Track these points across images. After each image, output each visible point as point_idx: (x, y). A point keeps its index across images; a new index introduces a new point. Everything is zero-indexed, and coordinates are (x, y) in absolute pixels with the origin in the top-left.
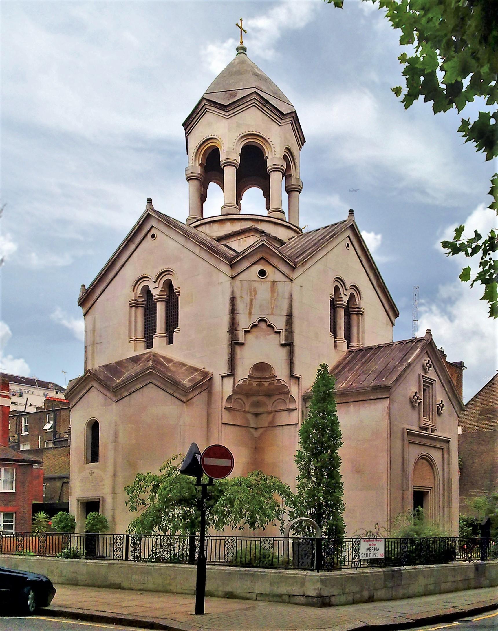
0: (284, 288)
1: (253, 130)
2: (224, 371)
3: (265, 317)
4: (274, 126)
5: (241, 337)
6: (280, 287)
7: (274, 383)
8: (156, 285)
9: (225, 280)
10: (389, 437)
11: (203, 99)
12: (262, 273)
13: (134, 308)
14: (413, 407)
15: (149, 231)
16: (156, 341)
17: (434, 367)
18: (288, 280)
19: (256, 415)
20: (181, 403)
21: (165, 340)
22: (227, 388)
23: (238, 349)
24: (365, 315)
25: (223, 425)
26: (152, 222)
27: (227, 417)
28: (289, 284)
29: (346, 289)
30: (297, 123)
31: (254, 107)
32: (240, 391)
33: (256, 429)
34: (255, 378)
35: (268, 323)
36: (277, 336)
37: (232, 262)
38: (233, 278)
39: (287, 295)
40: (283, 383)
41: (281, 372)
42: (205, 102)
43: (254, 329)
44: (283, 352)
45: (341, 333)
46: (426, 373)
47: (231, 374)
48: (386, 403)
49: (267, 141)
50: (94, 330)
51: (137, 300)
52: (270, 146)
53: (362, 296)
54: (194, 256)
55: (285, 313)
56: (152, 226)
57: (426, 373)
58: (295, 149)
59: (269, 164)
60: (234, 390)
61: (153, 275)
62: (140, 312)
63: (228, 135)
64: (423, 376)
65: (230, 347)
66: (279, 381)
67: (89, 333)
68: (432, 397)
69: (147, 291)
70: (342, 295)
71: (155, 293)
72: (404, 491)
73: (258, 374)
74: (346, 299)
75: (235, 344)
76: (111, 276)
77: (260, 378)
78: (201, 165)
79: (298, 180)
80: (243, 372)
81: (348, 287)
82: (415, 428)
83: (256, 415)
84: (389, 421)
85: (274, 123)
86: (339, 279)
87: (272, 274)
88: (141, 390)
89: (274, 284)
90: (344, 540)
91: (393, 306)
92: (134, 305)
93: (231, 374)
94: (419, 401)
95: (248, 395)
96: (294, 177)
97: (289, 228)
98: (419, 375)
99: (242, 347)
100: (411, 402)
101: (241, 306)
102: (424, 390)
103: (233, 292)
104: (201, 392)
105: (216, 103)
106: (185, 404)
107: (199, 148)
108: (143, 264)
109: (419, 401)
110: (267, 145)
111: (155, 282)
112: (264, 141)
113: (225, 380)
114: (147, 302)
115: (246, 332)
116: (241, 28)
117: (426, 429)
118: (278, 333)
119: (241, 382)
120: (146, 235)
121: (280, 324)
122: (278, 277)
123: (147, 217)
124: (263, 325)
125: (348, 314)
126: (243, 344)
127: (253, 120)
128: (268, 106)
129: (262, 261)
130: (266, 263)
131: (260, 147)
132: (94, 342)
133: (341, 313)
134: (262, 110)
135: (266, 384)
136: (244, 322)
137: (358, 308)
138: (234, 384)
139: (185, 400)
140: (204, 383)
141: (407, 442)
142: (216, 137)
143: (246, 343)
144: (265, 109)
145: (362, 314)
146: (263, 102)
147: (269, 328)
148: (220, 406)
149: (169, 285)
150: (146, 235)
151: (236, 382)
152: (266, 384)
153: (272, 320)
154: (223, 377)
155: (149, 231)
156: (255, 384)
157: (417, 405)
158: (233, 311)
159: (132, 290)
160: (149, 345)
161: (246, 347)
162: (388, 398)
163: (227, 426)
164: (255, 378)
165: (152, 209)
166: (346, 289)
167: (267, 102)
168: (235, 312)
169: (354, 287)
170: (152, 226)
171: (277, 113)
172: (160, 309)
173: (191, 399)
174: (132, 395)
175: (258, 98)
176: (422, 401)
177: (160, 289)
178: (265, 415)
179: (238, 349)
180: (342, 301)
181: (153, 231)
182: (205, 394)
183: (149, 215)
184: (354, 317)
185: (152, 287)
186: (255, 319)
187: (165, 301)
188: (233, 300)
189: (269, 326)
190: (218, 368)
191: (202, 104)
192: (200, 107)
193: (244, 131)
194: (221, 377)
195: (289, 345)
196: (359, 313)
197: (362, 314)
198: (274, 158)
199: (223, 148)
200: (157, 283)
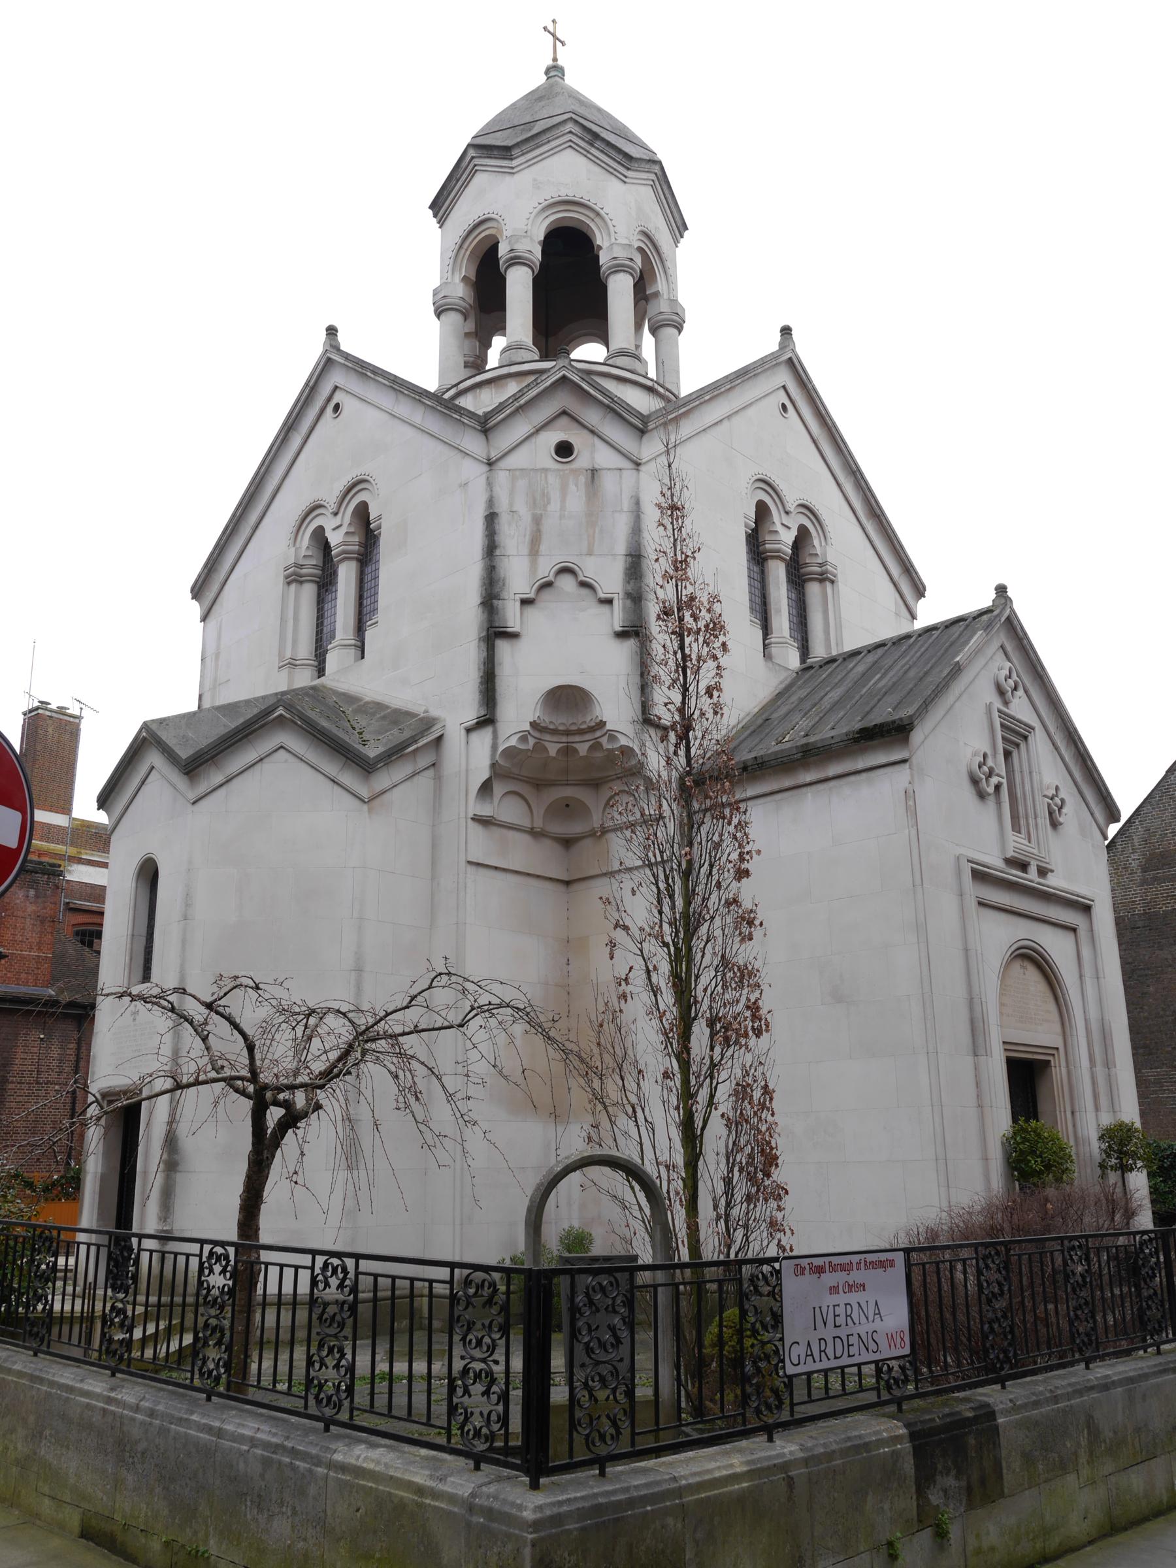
0: (617, 486)
1: (566, 193)
2: (471, 711)
3: (570, 559)
4: (614, 185)
5: (512, 615)
6: (608, 482)
7: (600, 745)
8: (337, 521)
9: (474, 472)
10: (918, 881)
11: (469, 145)
12: (564, 450)
13: (293, 586)
14: (982, 795)
15: (329, 399)
16: (333, 660)
17: (1026, 692)
18: (628, 465)
19: (567, 843)
20: (357, 802)
21: (352, 653)
22: (471, 758)
23: (502, 646)
24: (841, 585)
25: (469, 868)
26: (337, 377)
27: (480, 844)
28: (629, 475)
29: (787, 513)
30: (665, 187)
31: (570, 150)
32: (517, 772)
33: (567, 883)
34: (555, 732)
35: (581, 578)
36: (605, 609)
37: (485, 426)
38: (490, 464)
39: (626, 504)
40: (623, 741)
41: (615, 710)
42: (472, 153)
43: (546, 594)
44: (622, 654)
45: (782, 622)
46: (1006, 703)
47: (487, 721)
48: (901, 776)
49: (598, 214)
50: (217, 655)
51: (301, 566)
52: (608, 229)
53: (828, 535)
54: (410, 432)
55: (621, 548)
56: (336, 387)
57: (1006, 703)
58: (663, 237)
59: (604, 259)
60: (493, 766)
61: (331, 500)
62: (309, 592)
63: (519, 211)
64: (999, 711)
65: (483, 646)
66: (612, 737)
67: (208, 660)
68: (1030, 773)
69: (320, 537)
70: (779, 528)
71: (335, 539)
72: (977, 1047)
73: (561, 721)
74: (787, 538)
75: (495, 633)
76: (253, 517)
77: (568, 733)
78: (465, 279)
79: (674, 302)
80: (519, 711)
81: (791, 507)
82: (993, 860)
83: (567, 843)
84: (914, 832)
85: (613, 178)
86: (766, 484)
87: (590, 453)
88: (258, 766)
89: (593, 475)
90: (265, 1256)
91: (908, 568)
92: (294, 578)
93: (487, 721)
94: (994, 780)
95: (539, 785)
96: (666, 297)
97: (650, 390)
98: (989, 708)
99: (514, 641)
100: (975, 781)
101: (513, 540)
102: (1007, 754)
103: (491, 502)
104: (414, 775)
105: (493, 149)
106: (365, 807)
107: (461, 247)
108: (314, 480)
109: (994, 780)
110: (597, 219)
111: (336, 514)
112: (592, 215)
113: (475, 736)
114: (323, 570)
115: (525, 602)
116: (553, 35)
117: (1024, 866)
118: (609, 602)
119: (513, 742)
120: (322, 410)
121: (612, 581)
122: (604, 457)
123: (326, 365)
124: (567, 584)
125: (798, 578)
126: (515, 636)
127: (566, 174)
128: (598, 144)
129: (564, 420)
130: (576, 425)
131: (589, 234)
132: (215, 680)
133: (778, 572)
134: (586, 154)
135: (583, 749)
136: (518, 578)
137: (821, 565)
138: (494, 747)
139: (364, 793)
140: (411, 742)
141: (974, 904)
142: (493, 216)
143: (523, 633)
144: (593, 151)
145: (832, 582)
146: (588, 137)
147: (585, 592)
148: (463, 815)
149: (362, 512)
150: (322, 410)
151: (500, 740)
152: (583, 749)
153: (589, 569)
154: (469, 730)
155: (329, 399)
156: (553, 750)
157: (991, 790)
158: (491, 548)
159: (292, 541)
160: (321, 671)
161: (523, 644)
162: (904, 761)
163: (482, 871)
164: (555, 732)
165: (337, 348)
166: (787, 513)
167: (596, 136)
168: (498, 552)
169: (807, 509)
170: (336, 387)
171: (619, 157)
172: (346, 574)
173: (384, 792)
174: (235, 781)
175: (576, 130)
176: (1004, 781)
177: (344, 529)
178: (588, 842)
179: (502, 646)
180: (779, 542)
181: (338, 397)
182: (425, 781)
183: (329, 359)
184: (813, 589)
185: (328, 522)
186: (546, 569)
187: (358, 560)
188: (491, 519)
189: (584, 585)
190: (456, 708)
191: (468, 159)
192: (464, 164)
193: (551, 193)
194: (463, 732)
195: (637, 634)
196: (824, 578)
197: (832, 582)
198: (614, 243)
199: (505, 233)
200: (340, 515)
